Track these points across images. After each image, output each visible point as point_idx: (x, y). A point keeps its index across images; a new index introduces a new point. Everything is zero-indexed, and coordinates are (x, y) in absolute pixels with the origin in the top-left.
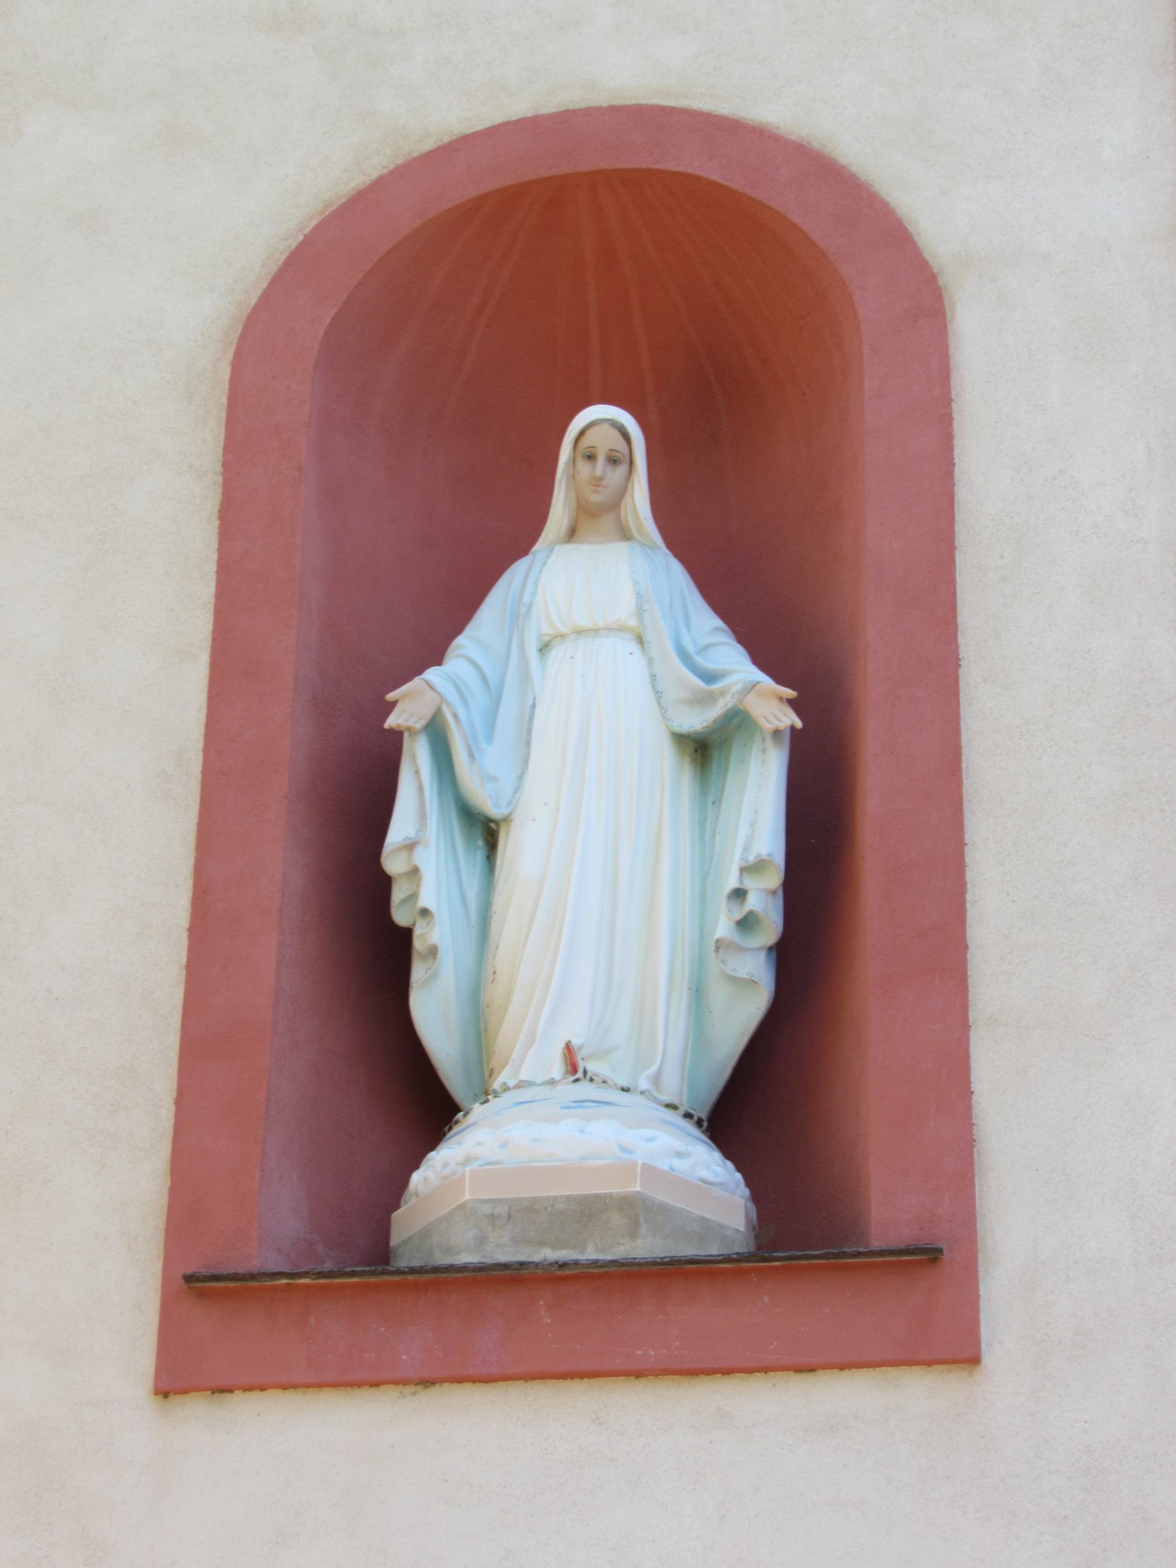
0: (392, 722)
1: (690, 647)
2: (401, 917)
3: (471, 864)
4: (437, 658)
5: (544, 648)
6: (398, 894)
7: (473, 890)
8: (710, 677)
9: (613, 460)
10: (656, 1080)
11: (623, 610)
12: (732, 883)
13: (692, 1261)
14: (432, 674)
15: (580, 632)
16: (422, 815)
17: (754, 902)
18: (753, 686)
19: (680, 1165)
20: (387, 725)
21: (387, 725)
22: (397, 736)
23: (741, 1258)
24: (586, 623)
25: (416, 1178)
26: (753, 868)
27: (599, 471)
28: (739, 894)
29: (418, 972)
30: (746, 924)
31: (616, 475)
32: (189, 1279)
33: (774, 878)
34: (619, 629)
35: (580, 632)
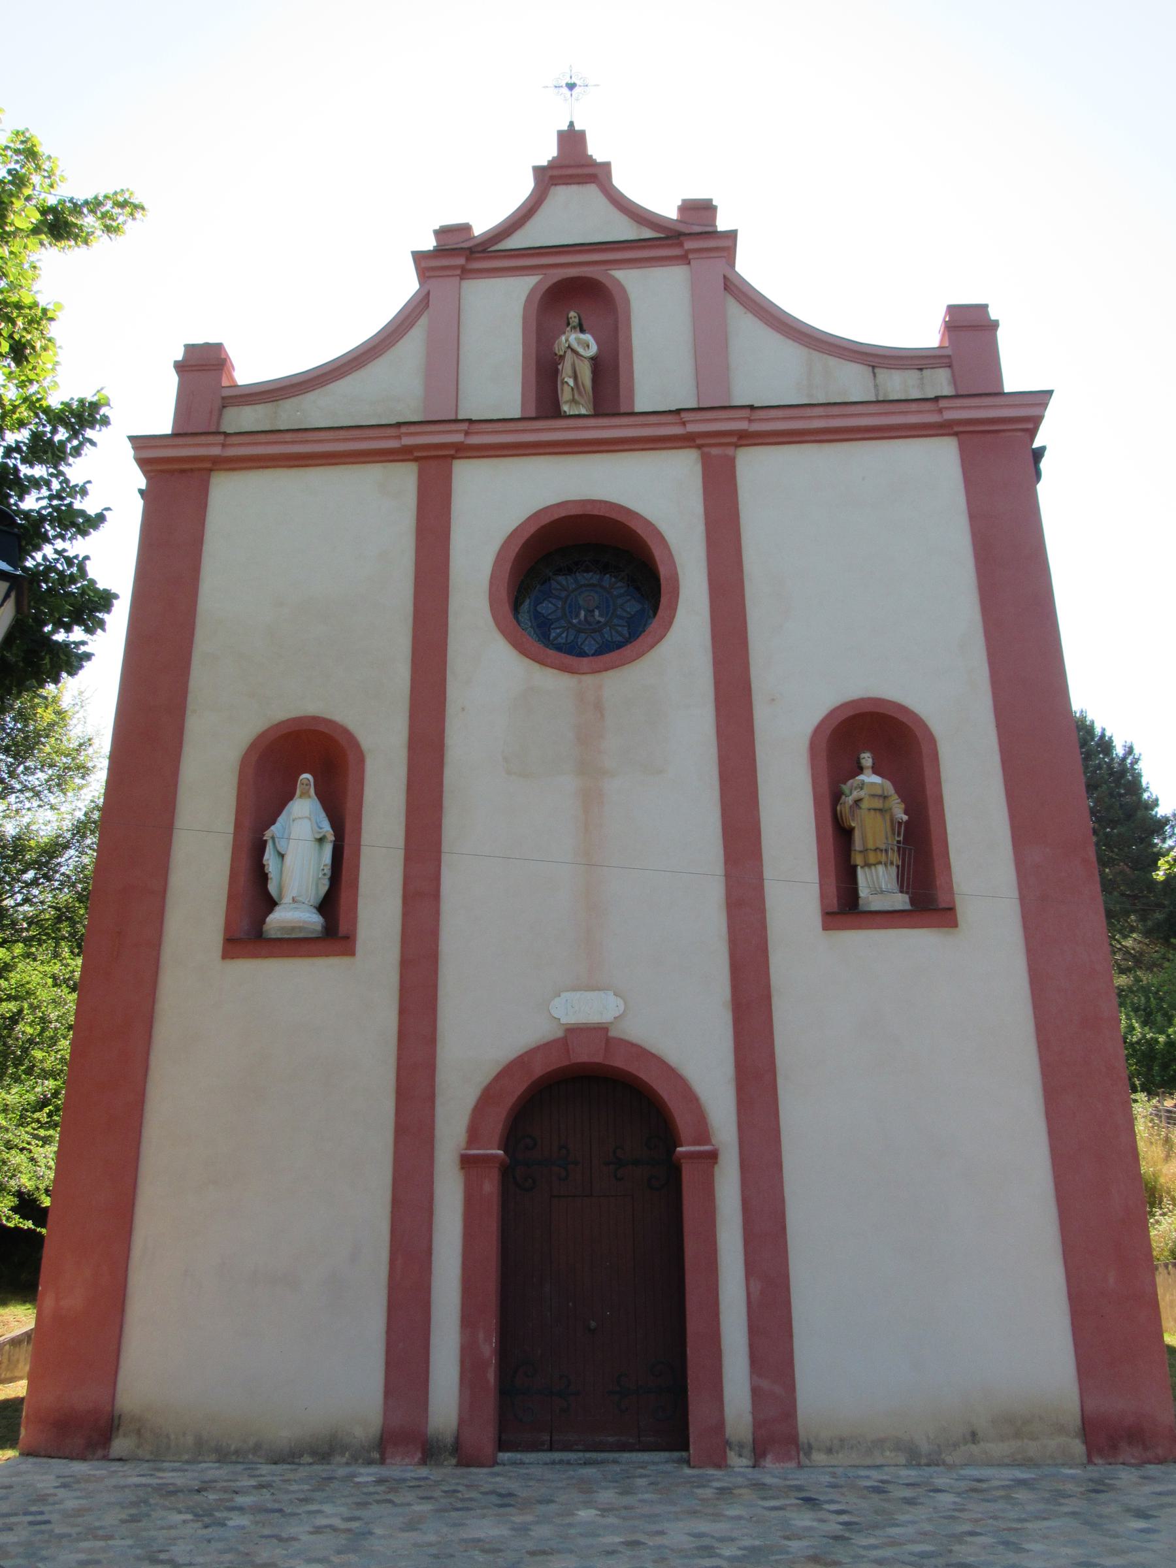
0: (265, 838)
1: (318, 821)
2: (266, 871)
3: (278, 860)
4: (274, 823)
5: (294, 820)
6: (266, 868)
7: (279, 866)
8: (321, 828)
9: (307, 785)
10: (309, 901)
11: (307, 814)
12: (322, 868)
13: (416, 322)
14: (273, 828)
15: (300, 818)
16: (270, 854)
17: (325, 871)
18: (327, 831)
19: (310, 919)
20: (1034, 446)
21: (1034, 446)
22: (266, 841)
23: (317, 939)
24: (300, 816)
25: (268, 919)
26: (325, 865)
27: (1167, 1178)
28: (323, 870)
29: (269, 881)
30: (324, 874)
31: (307, 787)
32: (228, 940)
33: (329, 867)
34: (306, 817)
35: (300, 818)
